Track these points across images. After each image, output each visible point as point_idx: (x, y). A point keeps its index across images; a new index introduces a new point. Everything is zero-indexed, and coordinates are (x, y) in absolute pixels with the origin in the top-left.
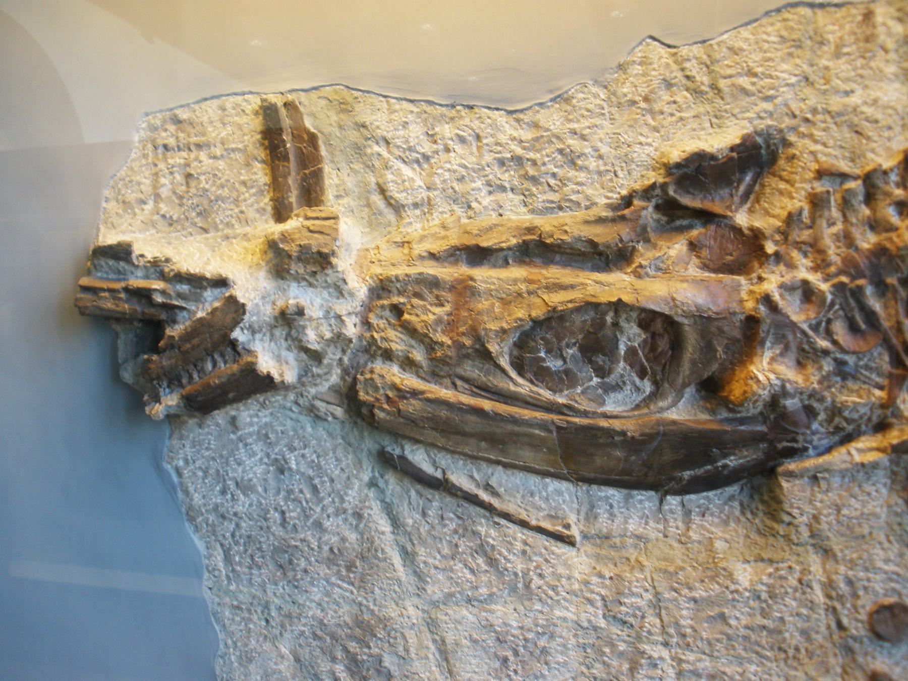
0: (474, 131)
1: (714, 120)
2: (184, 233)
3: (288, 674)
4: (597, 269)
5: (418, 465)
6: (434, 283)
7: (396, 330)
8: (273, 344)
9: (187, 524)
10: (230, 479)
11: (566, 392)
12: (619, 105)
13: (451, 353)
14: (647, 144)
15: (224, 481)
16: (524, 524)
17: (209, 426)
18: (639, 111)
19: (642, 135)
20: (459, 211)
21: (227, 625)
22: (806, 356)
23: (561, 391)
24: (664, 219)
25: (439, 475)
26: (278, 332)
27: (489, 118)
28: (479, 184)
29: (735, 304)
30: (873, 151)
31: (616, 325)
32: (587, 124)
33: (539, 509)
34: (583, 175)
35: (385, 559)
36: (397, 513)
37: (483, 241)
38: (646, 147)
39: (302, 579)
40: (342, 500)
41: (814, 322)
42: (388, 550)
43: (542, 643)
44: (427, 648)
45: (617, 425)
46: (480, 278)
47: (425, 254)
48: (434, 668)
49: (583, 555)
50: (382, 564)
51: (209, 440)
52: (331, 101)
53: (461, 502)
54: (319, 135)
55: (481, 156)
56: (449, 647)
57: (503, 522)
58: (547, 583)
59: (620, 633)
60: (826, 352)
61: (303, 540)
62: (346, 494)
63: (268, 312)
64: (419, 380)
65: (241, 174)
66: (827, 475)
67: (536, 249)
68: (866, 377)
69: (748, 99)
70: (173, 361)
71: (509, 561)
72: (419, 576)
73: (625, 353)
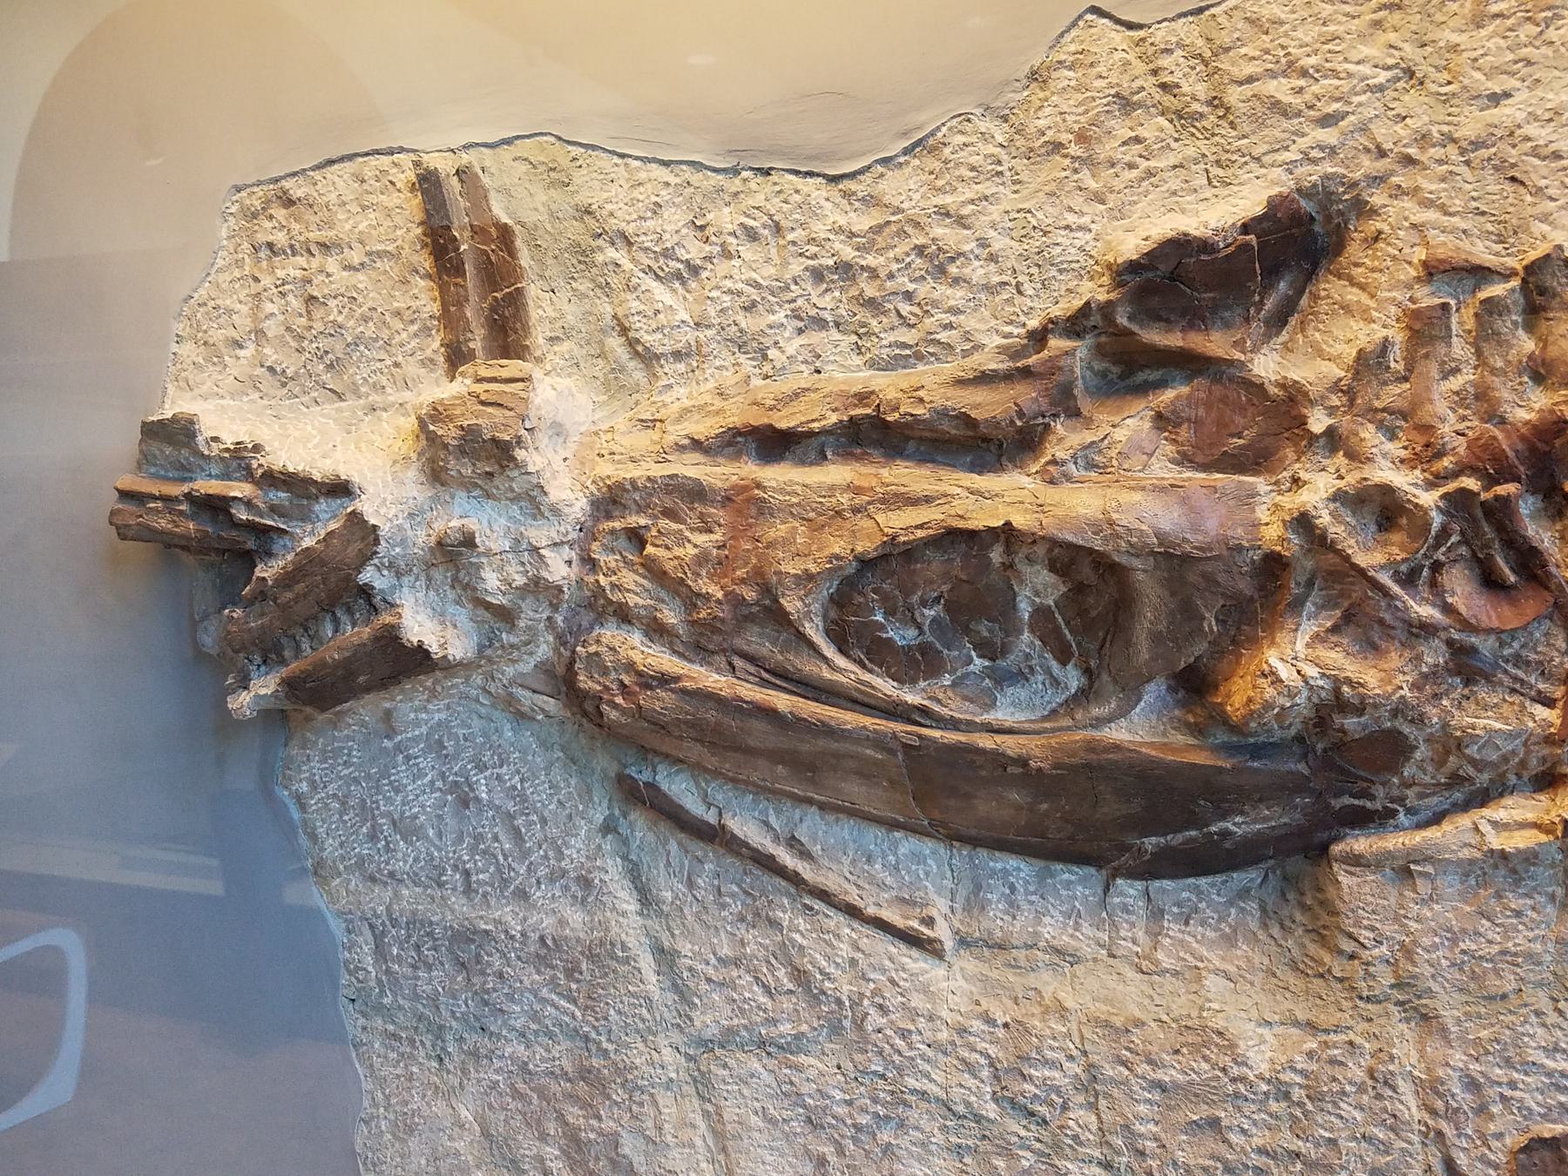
0: (771, 216)
1: (1216, 171)
2: (305, 399)
3: (470, 1158)
4: (979, 468)
6: (697, 493)
8: (432, 593)
10: (382, 816)
11: (922, 684)
12: (1029, 154)
14: (1080, 228)
15: (374, 818)
16: (853, 912)
18: (1067, 161)
19: (1070, 209)
20: (747, 365)
21: (377, 1066)
24: (1116, 370)
25: (711, 817)
26: (437, 575)
27: (797, 191)
28: (780, 316)
29: (1240, 531)
30: (1545, 218)
31: (1009, 566)
32: (970, 195)
33: (882, 886)
34: (960, 294)
35: (627, 961)
37: (782, 418)
38: (1079, 234)
39: (495, 990)
40: (560, 855)
41: (1404, 568)
43: (885, 1136)
44: (693, 1126)
47: (686, 442)
48: (704, 1165)
49: (959, 976)
50: (623, 969)
51: (350, 749)
52: (535, 167)
53: (750, 866)
54: (517, 229)
55: (785, 264)
56: (729, 1127)
57: (818, 905)
58: (892, 1022)
59: (1023, 1133)
60: (1426, 629)
61: (497, 922)
62: (565, 843)
63: (422, 538)
66: (1430, 869)
67: (871, 434)
68: (1515, 679)
69: (1285, 124)
70: (265, 620)
71: (827, 976)
72: (683, 993)
73: (1031, 617)
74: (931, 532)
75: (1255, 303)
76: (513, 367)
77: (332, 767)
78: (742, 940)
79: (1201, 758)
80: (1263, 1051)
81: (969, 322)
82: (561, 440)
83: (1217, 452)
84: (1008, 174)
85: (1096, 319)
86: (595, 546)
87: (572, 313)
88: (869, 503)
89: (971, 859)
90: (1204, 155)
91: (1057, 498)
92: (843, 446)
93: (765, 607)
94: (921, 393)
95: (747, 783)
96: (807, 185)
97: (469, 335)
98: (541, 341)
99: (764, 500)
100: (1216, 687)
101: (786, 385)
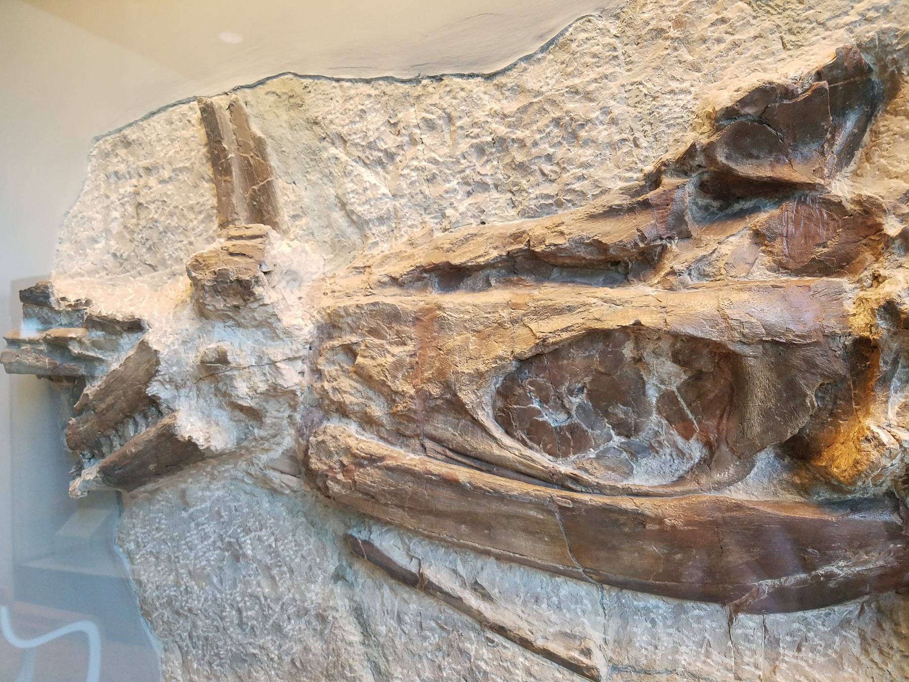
0: (444, 110)
1: (788, 37)
2: (133, 272)
4: (611, 283)
5: (386, 553)
6: (394, 316)
7: (350, 378)
8: (201, 401)
9: (142, 620)
11: (572, 457)
12: (638, 41)
13: (416, 405)
14: (683, 91)
15: (176, 569)
16: (525, 644)
17: (159, 501)
18: (668, 43)
19: (673, 78)
20: (431, 222)
23: (566, 455)
24: (716, 204)
25: (413, 567)
27: (462, 89)
31: (638, 360)
32: (593, 76)
33: (548, 622)
34: (589, 152)
36: (368, 617)
37: (456, 257)
42: (357, 666)
45: (646, 506)
46: (451, 306)
47: (386, 279)
51: (161, 519)
52: (280, 97)
54: (269, 141)
55: (456, 144)
57: (498, 638)
61: (262, 648)
63: (191, 358)
64: (382, 443)
65: (189, 197)
67: (528, 263)
70: (89, 424)
73: (658, 401)
74: (574, 333)
75: (828, 141)
76: (258, 228)
77: (150, 531)
78: (439, 667)
79: (808, 514)
81: (597, 173)
82: (297, 284)
83: (806, 260)
84: (622, 57)
85: (700, 159)
86: (321, 360)
87: (307, 197)
88: (524, 315)
89: (618, 598)
90: (778, 26)
91: (677, 301)
92: (504, 276)
93: (447, 401)
94: (562, 228)
95: (440, 540)
96: (470, 83)
97: (235, 216)
98: (286, 218)
99: (443, 318)
100: (819, 453)
101: (459, 234)
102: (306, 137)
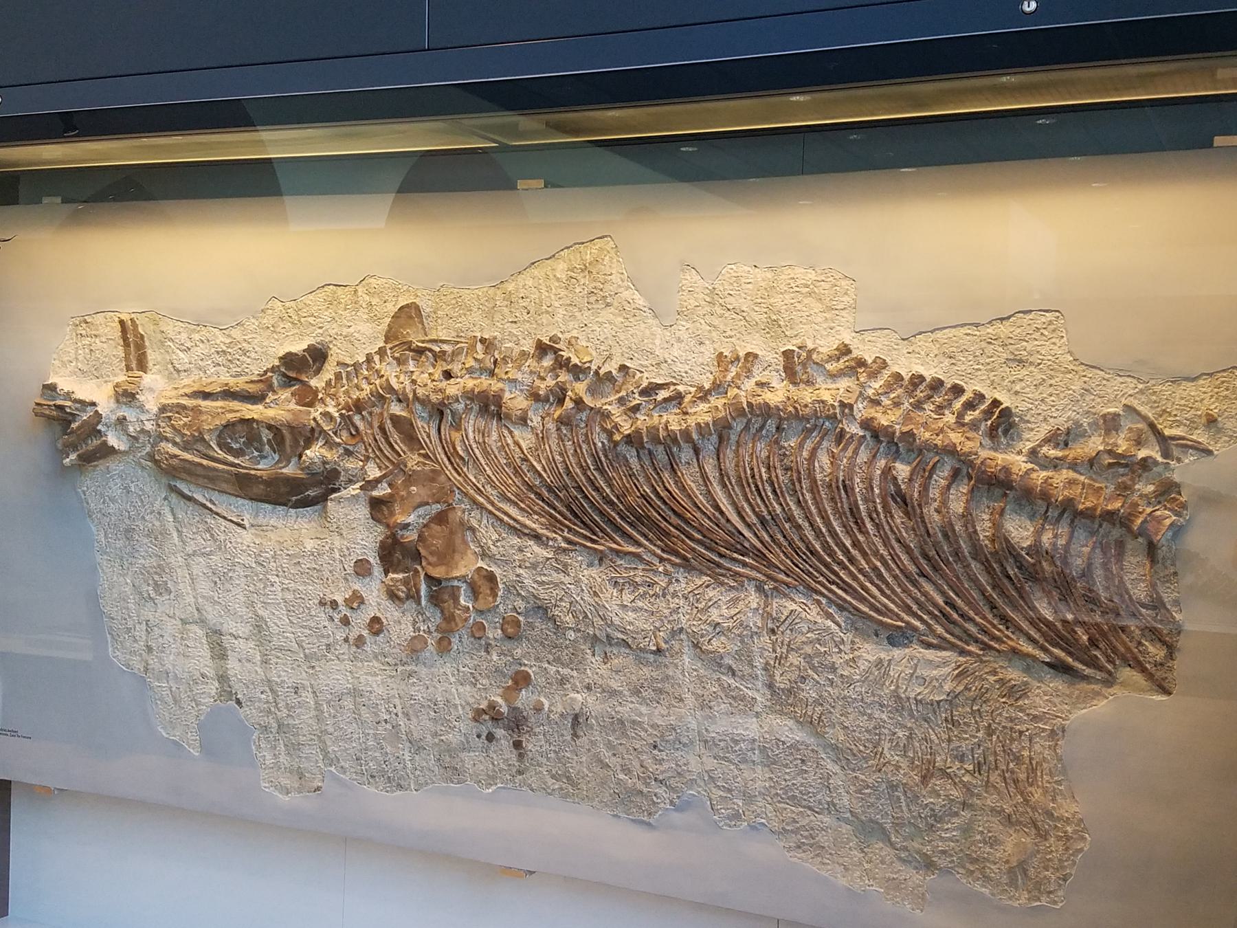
6: (184, 407)
16: (225, 518)
22: (329, 444)
60: (339, 444)
63: (114, 417)
67: (229, 394)
80: (310, 545)
101: (209, 380)
102: (159, 336)
